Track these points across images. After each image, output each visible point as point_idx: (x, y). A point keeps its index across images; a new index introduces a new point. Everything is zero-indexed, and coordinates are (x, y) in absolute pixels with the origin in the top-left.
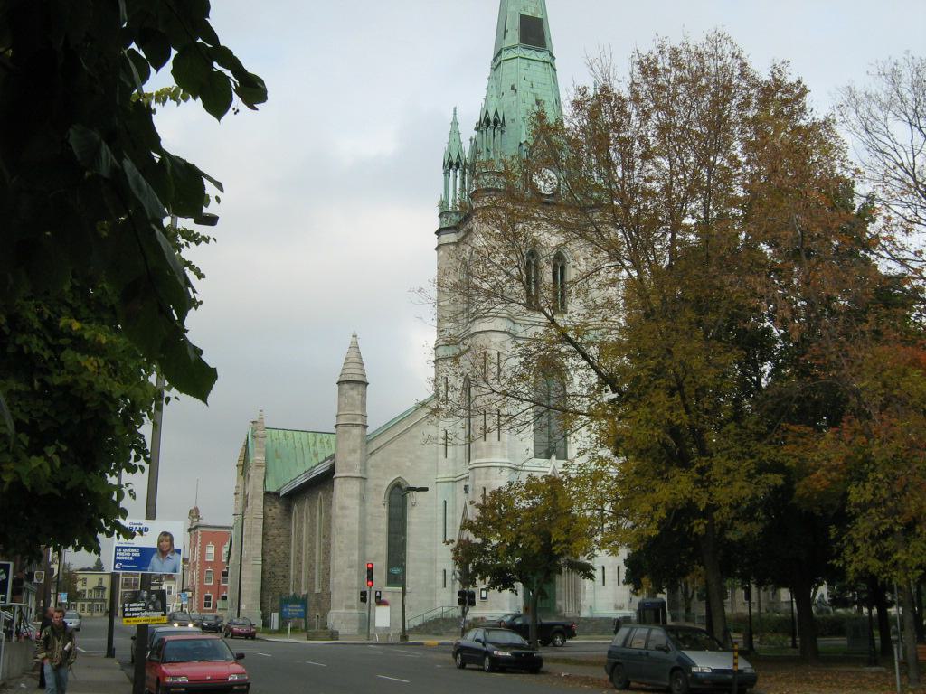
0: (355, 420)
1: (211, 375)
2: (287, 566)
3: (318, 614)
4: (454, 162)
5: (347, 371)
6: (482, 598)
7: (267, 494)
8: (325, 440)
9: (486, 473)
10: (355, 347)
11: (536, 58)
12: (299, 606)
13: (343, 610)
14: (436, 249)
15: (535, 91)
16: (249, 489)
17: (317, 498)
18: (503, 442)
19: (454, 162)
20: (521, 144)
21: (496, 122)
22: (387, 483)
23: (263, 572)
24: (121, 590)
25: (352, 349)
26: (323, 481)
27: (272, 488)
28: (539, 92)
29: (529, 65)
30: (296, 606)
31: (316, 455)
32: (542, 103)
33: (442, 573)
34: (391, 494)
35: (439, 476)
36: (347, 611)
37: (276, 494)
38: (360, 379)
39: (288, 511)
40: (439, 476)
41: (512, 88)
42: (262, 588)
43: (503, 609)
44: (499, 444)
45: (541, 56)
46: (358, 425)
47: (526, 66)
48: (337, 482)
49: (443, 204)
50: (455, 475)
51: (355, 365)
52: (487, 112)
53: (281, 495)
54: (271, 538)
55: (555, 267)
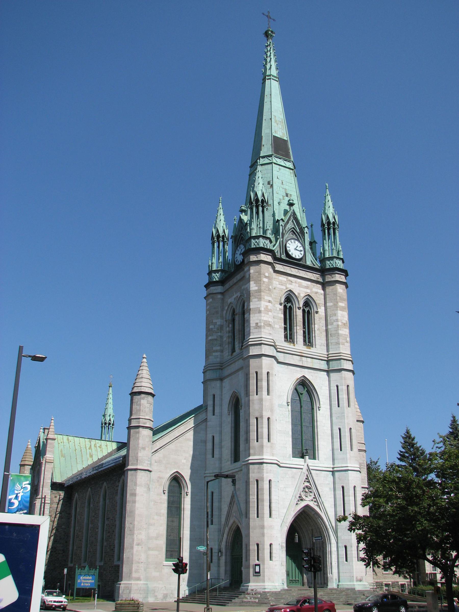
6: (256, 572)
8: (98, 445)
9: (258, 468)
11: (284, 165)
12: (91, 578)
15: (285, 187)
17: (101, 488)
18: (272, 444)
28: (287, 187)
29: (280, 169)
30: (88, 578)
31: (91, 456)
35: (206, 472)
41: (269, 183)
43: (273, 582)
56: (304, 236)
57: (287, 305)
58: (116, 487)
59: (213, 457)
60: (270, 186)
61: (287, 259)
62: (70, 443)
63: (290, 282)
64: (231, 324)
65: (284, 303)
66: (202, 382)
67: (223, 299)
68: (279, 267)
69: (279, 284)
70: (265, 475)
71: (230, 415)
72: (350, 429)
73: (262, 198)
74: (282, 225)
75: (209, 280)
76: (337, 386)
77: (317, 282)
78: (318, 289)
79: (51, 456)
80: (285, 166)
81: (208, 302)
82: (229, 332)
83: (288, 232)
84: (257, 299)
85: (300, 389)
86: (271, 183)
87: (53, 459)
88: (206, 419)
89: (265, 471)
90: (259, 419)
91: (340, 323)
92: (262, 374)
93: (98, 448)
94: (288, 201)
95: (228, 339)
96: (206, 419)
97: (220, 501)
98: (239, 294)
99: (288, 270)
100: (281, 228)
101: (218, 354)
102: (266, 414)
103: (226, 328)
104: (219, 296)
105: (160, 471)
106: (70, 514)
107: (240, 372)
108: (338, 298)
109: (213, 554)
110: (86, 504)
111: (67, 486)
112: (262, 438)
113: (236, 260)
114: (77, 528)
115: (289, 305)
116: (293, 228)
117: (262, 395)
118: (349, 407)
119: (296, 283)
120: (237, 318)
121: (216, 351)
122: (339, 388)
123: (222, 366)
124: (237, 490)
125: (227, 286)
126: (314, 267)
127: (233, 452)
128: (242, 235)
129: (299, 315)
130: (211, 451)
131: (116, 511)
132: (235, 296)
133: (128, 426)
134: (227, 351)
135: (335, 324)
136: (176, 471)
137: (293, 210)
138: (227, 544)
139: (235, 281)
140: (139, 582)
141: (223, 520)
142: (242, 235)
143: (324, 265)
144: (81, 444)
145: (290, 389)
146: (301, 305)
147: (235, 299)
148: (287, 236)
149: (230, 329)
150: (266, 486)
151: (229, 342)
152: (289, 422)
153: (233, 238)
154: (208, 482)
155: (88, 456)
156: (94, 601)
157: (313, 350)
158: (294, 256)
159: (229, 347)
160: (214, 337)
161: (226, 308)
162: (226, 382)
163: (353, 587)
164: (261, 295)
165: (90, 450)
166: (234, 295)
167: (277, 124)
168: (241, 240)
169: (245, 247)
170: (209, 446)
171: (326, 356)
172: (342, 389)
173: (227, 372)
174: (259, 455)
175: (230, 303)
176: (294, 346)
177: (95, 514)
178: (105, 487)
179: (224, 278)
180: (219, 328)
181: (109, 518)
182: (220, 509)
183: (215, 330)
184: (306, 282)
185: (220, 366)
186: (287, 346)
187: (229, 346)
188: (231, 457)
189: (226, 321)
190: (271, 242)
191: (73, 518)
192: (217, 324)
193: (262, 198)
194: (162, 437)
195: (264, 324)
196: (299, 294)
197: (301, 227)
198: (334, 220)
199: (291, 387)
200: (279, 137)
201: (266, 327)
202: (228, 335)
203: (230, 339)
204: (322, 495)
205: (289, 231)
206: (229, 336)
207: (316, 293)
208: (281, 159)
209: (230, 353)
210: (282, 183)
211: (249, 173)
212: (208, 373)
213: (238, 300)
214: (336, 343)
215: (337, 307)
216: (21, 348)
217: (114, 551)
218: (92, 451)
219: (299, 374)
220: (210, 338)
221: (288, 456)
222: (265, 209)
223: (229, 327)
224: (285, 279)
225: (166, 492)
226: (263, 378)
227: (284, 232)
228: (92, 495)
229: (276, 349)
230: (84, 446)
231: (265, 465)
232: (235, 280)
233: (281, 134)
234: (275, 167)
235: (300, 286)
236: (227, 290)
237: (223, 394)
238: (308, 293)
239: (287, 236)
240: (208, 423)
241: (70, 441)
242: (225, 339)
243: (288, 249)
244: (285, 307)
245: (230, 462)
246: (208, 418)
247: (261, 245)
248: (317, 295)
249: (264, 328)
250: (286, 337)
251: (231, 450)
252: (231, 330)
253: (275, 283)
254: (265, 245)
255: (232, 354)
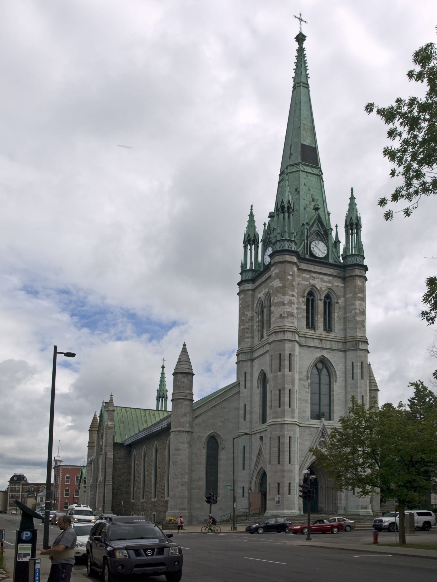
0: (186, 396)
1: (378, 113)
2: (128, 485)
3: (154, 513)
4: (252, 239)
5: (180, 366)
7: (116, 445)
10: (184, 351)
13: (178, 511)
14: (238, 294)
15: (312, 192)
16: (103, 443)
19: (252, 239)
20: (303, 224)
21: (289, 208)
22: (207, 435)
23: (113, 489)
24: (9, 500)
25: (183, 353)
26: (166, 431)
27: (118, 440)
28: (314, 193)
31: (146, 422)
32: (315, 200)
33: (241, 489)
34: (208, 442)
35: (240, 431)
36: (180, 511)
37: (122, 445)
38: (187, 371)
39: (129, 453)
40: (240, 431)
41: (296, 190)
42: (113, 498)
43: (291, 510)
44: (290, 410)
45: (315, 171)
46: (187, 399)
47: (305, 176)
48: (172, 435)
49: (243, 266)
50: (250, 431)
51: (186, 363)
52: (249, 235)
53: (125, 445)
54: (118, 469)
55: (325, 303)
56: (328, 237)
57: (310, 298)
58: (165, 444)
59: (245, 420)
60: (297, 192)
61: (312, 258)
62: (128, 413)
63: (313, 278)
64: (260, 315)
65: (307, 296)
66: (236, 363)
67: (253, 295)
68: (303, 266)
69: (303, 280)
70: (286, 433)
71: (259, 388)
72: (363, 396)
73: (288, 205)
74: (307, 229)
75: (241, 279)
76: (353, 363)
77: (338, 277)
78: (338, 283)
79: (112, 423)
80: (312, 172)
81: (241, 297)
82: (259, 322)
83: (312, 234)
84: (281, 294)
85: (320, 366)
86: (298, 190)
87: (114, 425)
88: (239, 391)
89: (286, 429)
90: (281, 391)
91: (358, 311)
92: (284, 355)
93: (152, 416)
94: (314, 206)
95: (257, 328)
96: (239, 391)
97: (250, 453)
98: (267, 290)
99: (312, 268)
100: (306, 230)
101: (249, 340)
102: (288, 387)
103: (256, 318)
104: (250, 292)
105: (200, 432)
106: (130, 465)
107: (268, 354)
108: (357, 290)
109: (245, 491)
110: (143, 458)
111: (127, 445)
112: (284, 405)
113: (265, 261)
114: (136, 475)
115: (311, 298)
116: (318, 230)
117: (284, 372)
118: (362, 379)
119: (318, 278)
120: (265, 310)
121: (248, 338)
122: (354, 364)
123: (252, 350)
124: (263, 444)
125: (257, 283)
126: (337, 264)
127: (261, 416)
128: (271, 239)
129: (320, 305)
130: (243, 416)
131: (165, 462)
132: (263, 292)
133: (172, 399)
134: (257, 337)
135: (353, 312)
136: (213, 431)
137: (318, 214)
138: (256, 484)
139: (264, 279)
140: (184, 511)
141: (253, 466)
142: (271, 239)
143: (345, 262)
144: (137, 413)
145: (310, 366)
146: (323, 298)
147: (263, 294)
148: (311, 238)
149: (260, 319)
150: (287, 441)
151: (258, 330)
152: (308, 392)
153: (263, 241)
154: (234, 439)
155: (144, 422)
156: (110, 511)
157: (332, 334)
158: (317, 255)
159: (258, 334)
160: (245, 327)
161: (256, 302)
162: (256, 362)
163: (358, 513)
164: (285, 291)
165: (145, 418)
166: (263, 291)
167: (306, 132)
168: (269, 243)
169: (273, 249)
170: (242, 412)
171: (343, 339)
172: (357, 366)
173: (256, 354)
174: (281, 418)
175: (260, 298)
176: (315, 331)
177: (150, 465)
178: (156, 445)
179: (255, 276)
180: (250, 319)
181: (160, 467)
182: (250, 459)
183: (247, 320)
184: (328, 277)
185: (251, 350)
186: (311, 333)
187: (258, 333)
188: (260, 420)
189: (256, 313)
190: (296, 244)
191: (133, 468)
192: (249, 315)
193: (288, 205)
194: (200, 406)
195: (288, 314)
196: (321, 288)
197: (326, 229)
198: (357, 221)
199: (311, 365)
200: (307, 144)
201: (289, 317)
202: (257, 324)
203: (259, 328)
204: (59, 425)
205: (314, 233)
206: (258, 325)
207: (337, 286)
208: (309, 166)
209: (259, 339)
210: (309, 189)
211: (278, 181)
212: (240, 355)
213: (267, 294)
214: (353, 328)
215: (356, 298)
216: (56, 347)
217: (165, 491)
218: (146, 419)
219: (318, 354)
220: (242, 327)
221: (306, 418)
222: (291, 215)
223: (258, 317)
224: (308, 276)
225: (206, 447)
226: (286, 358)
227: (309, 234)
228: (147, 451)
229: (298, 335)
230: (140, 415)
231: (286, 426)
232: (264, 278)
233: (310, 142)
234: (303, 175)
235: (322, 281)
236: (257, 287)
237: (253, 371)
238: (329, 286)
239: (311, 238)
240: (241, 395)
241: (128, 412)
242: (255, 327)
243: (312, 249)
244: (308, 300)
245: (258, 424)
246: (241, 391)
247: (287, 248)
248: (338, 288)
249: (288, 318)
250: (308, 324)
251: (260, 415)
252: (261, 320)
253: (298, 280)
254: (290, 247)
255: (261, 340)
